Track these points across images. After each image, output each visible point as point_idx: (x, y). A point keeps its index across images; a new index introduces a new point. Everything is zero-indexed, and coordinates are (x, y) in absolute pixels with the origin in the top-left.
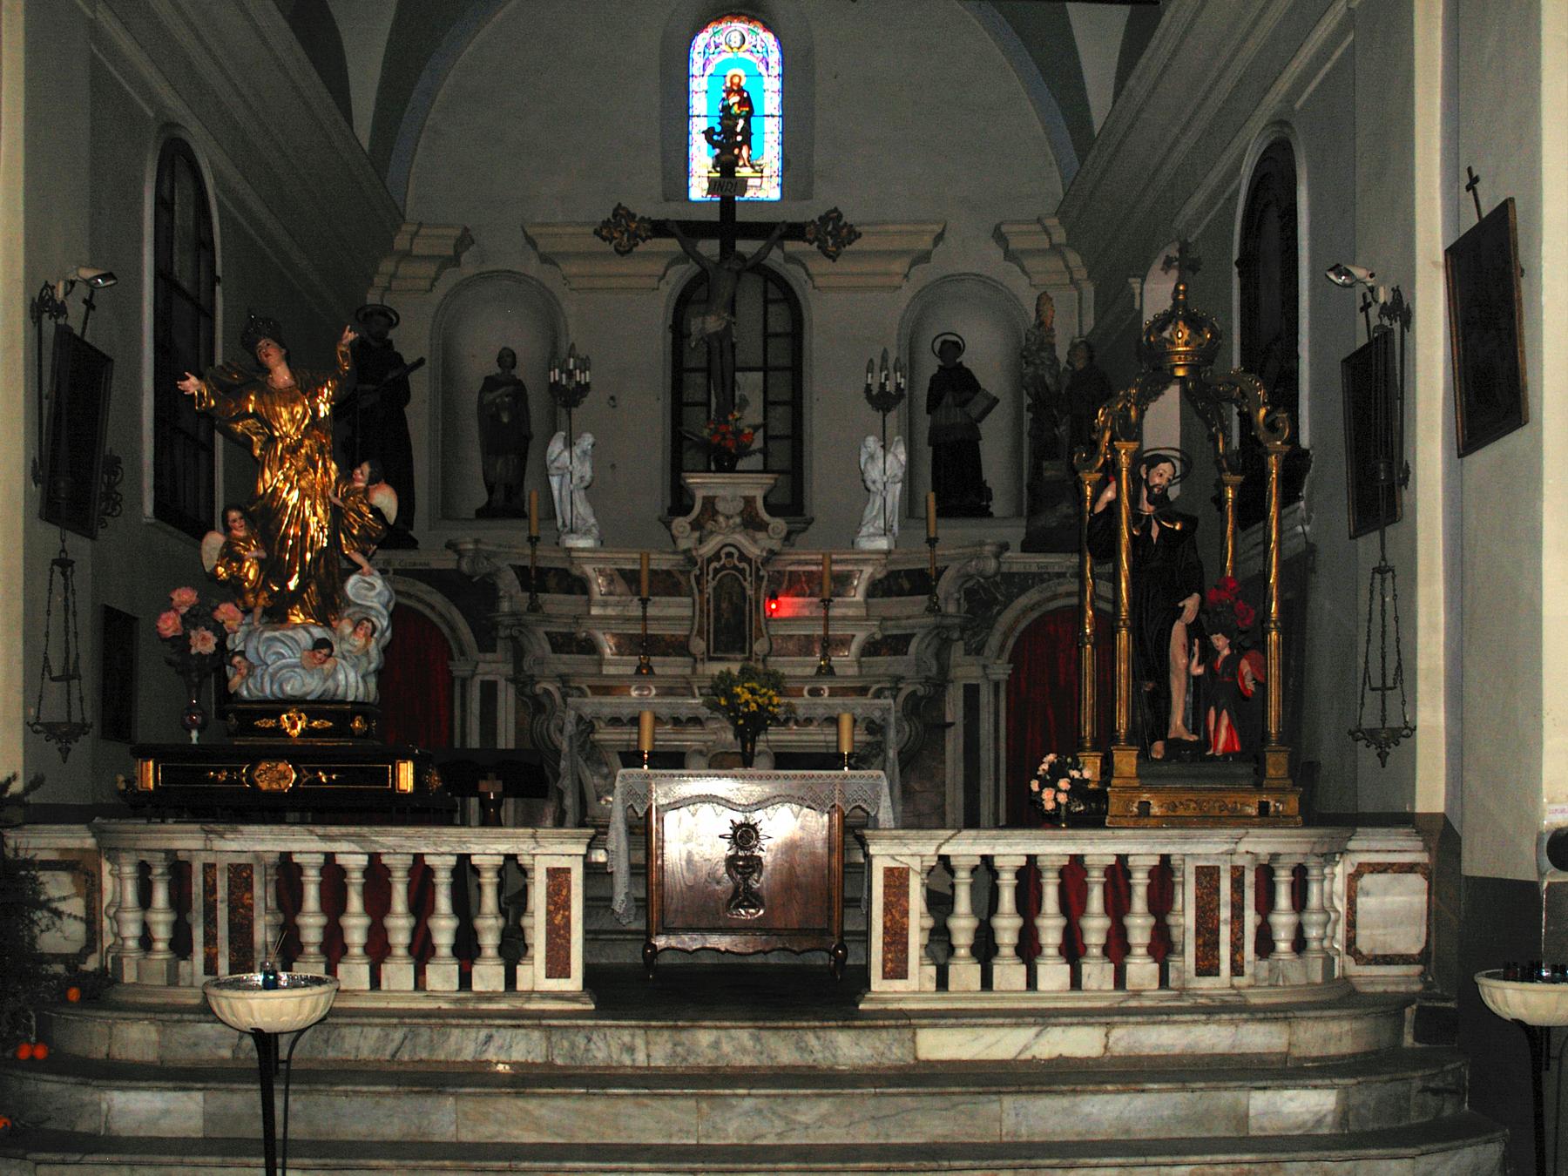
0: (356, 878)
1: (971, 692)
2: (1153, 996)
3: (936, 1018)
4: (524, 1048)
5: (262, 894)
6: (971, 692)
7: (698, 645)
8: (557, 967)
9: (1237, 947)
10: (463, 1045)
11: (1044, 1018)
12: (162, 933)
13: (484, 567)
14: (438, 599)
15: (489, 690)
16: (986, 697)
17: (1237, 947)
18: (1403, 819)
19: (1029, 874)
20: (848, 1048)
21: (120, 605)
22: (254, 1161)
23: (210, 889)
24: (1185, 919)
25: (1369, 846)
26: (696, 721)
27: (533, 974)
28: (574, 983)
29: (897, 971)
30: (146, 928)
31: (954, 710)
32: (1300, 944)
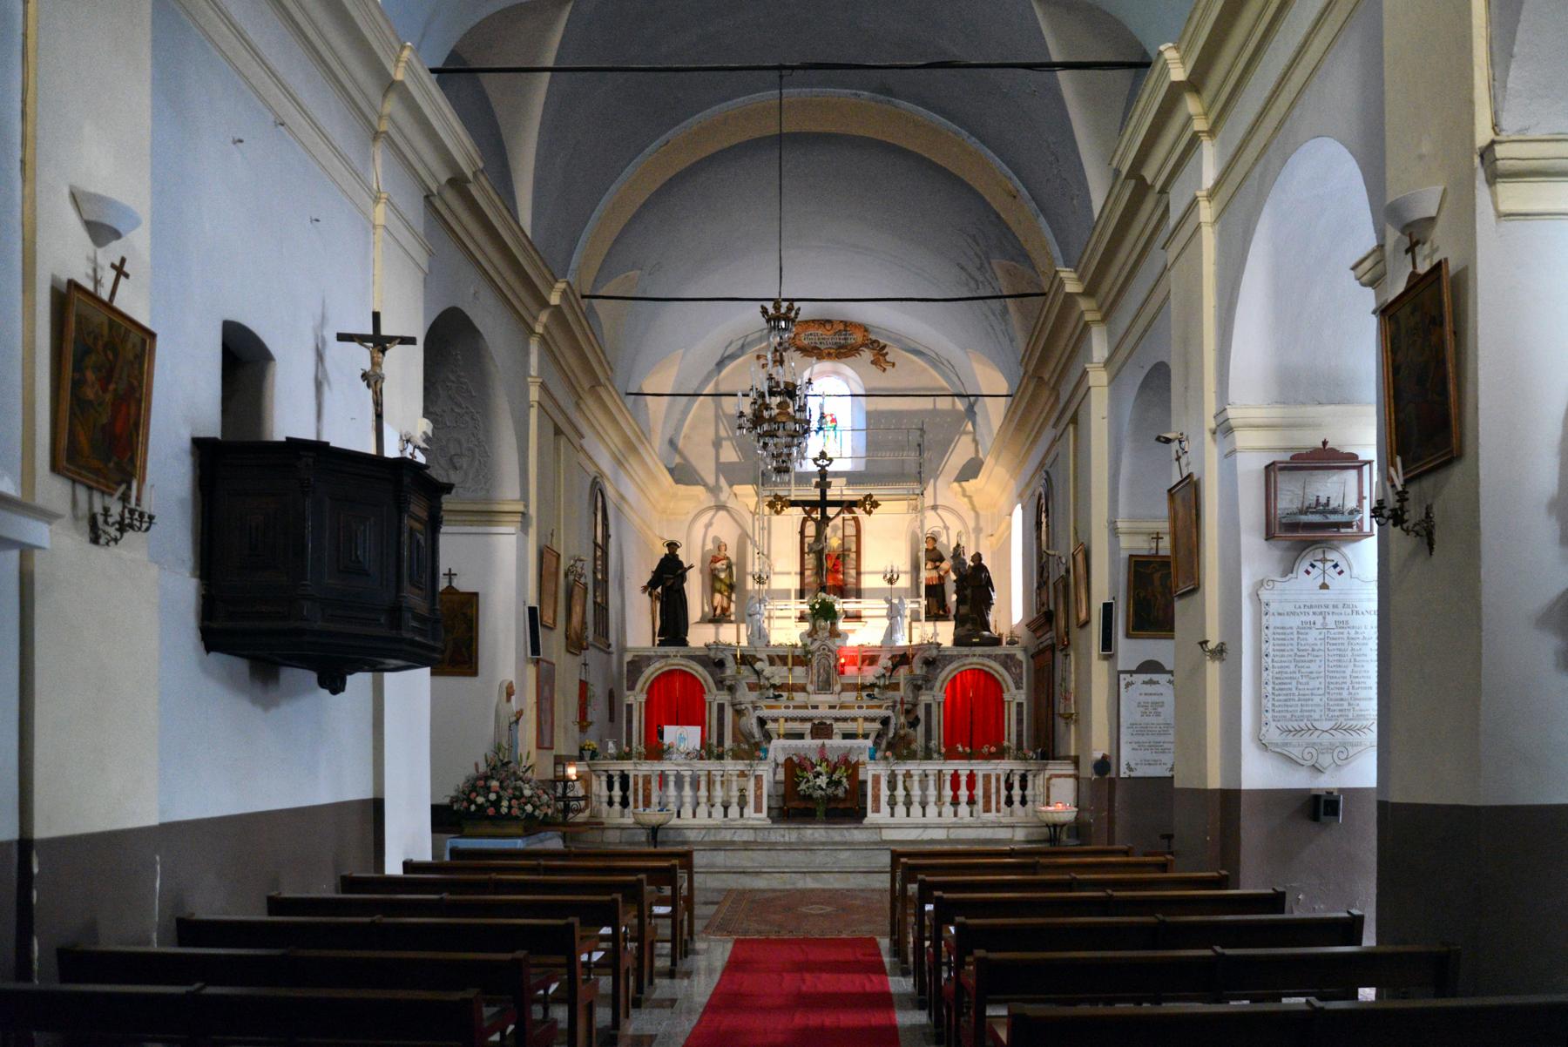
0: (688, 779)
1: (928, 706)
2: (967, 819)
3: (889, 827)
4: (748, 836)
5: (655, 784)
6: (928, 706)
7: (810, 688)
8: (758, 809)
9: (998, 803)
10: (727, 836)
11: (925, 827)
12: (617, 799)
13: (720, 655)
14: (700, 669)
15: (721, 707)
16: (934, 708)
17: (998, 803)
18: (1067, 758)
19: (908, 775)
20: (857, 835)
21: (1227, 646)
22: (714, 882)
23: (636, 784)
24: (979, 792)
25: (1055, 768)
26: (837, 720)
27: (749, 811)
28: (764, 814)
29: (877, 810)
30: (610, 798)
31: (921, 713)
32: (1023, 802)
